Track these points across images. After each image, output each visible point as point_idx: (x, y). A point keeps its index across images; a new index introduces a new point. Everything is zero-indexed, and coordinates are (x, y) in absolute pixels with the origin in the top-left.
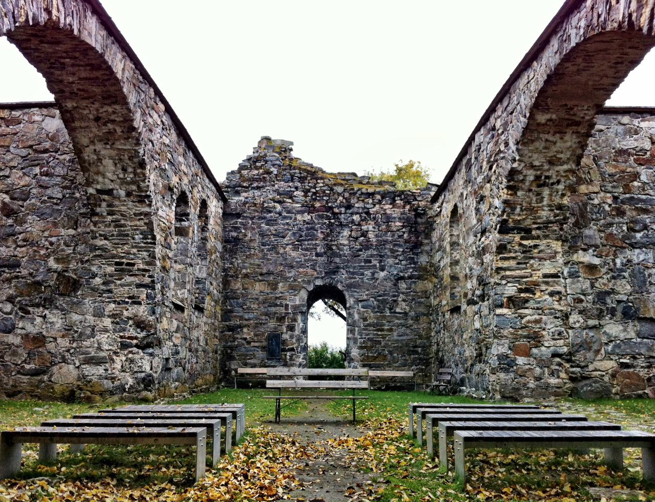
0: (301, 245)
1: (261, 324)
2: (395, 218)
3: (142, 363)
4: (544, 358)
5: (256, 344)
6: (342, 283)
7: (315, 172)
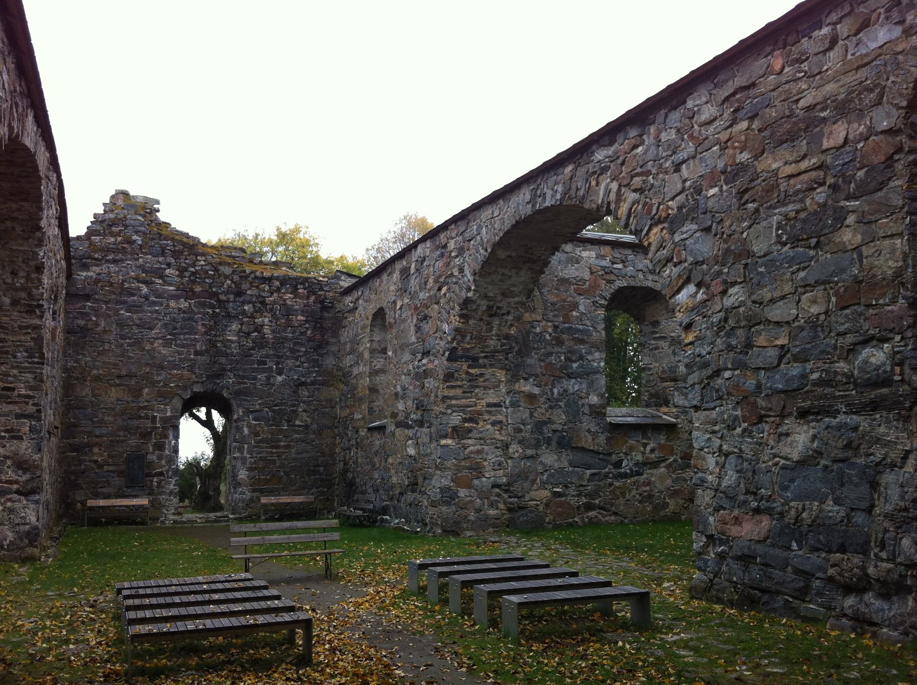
0: (175, 340)
1: (118, 441)
2: (296, 310)
3: (26, 513)
4: (484, 489)
5: (111, 468)
6: (228, 389)
7: (193, 245)
